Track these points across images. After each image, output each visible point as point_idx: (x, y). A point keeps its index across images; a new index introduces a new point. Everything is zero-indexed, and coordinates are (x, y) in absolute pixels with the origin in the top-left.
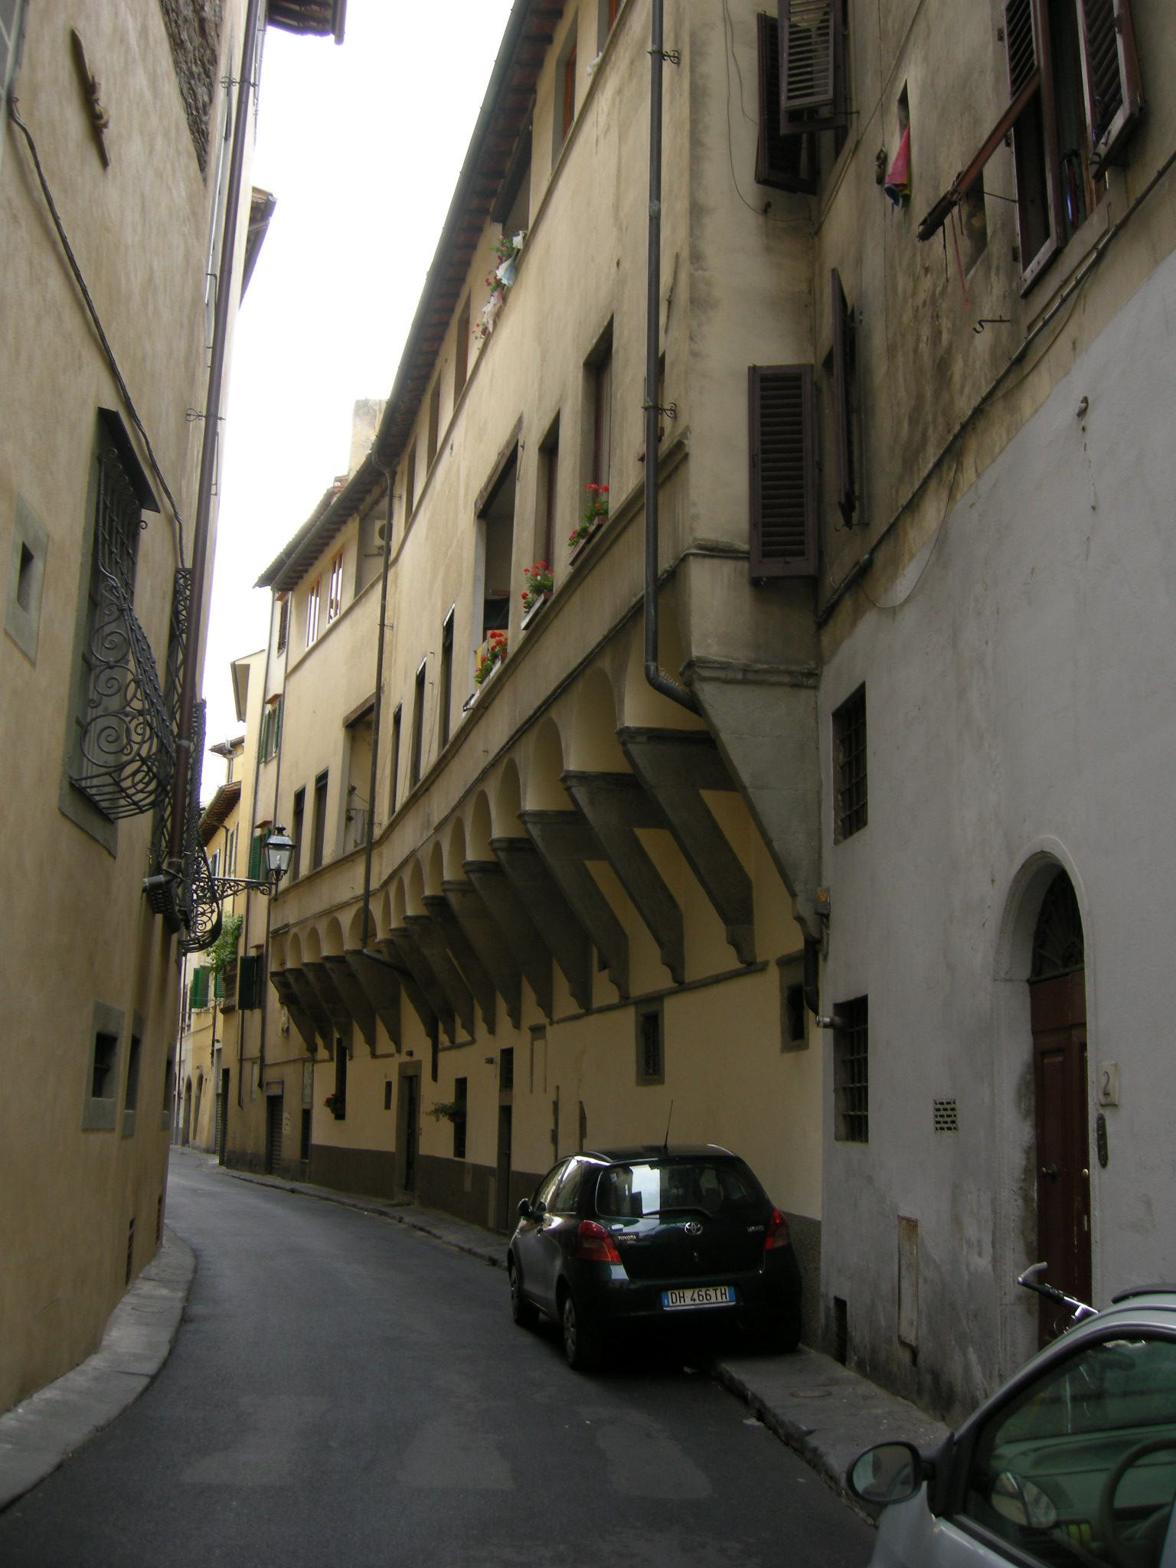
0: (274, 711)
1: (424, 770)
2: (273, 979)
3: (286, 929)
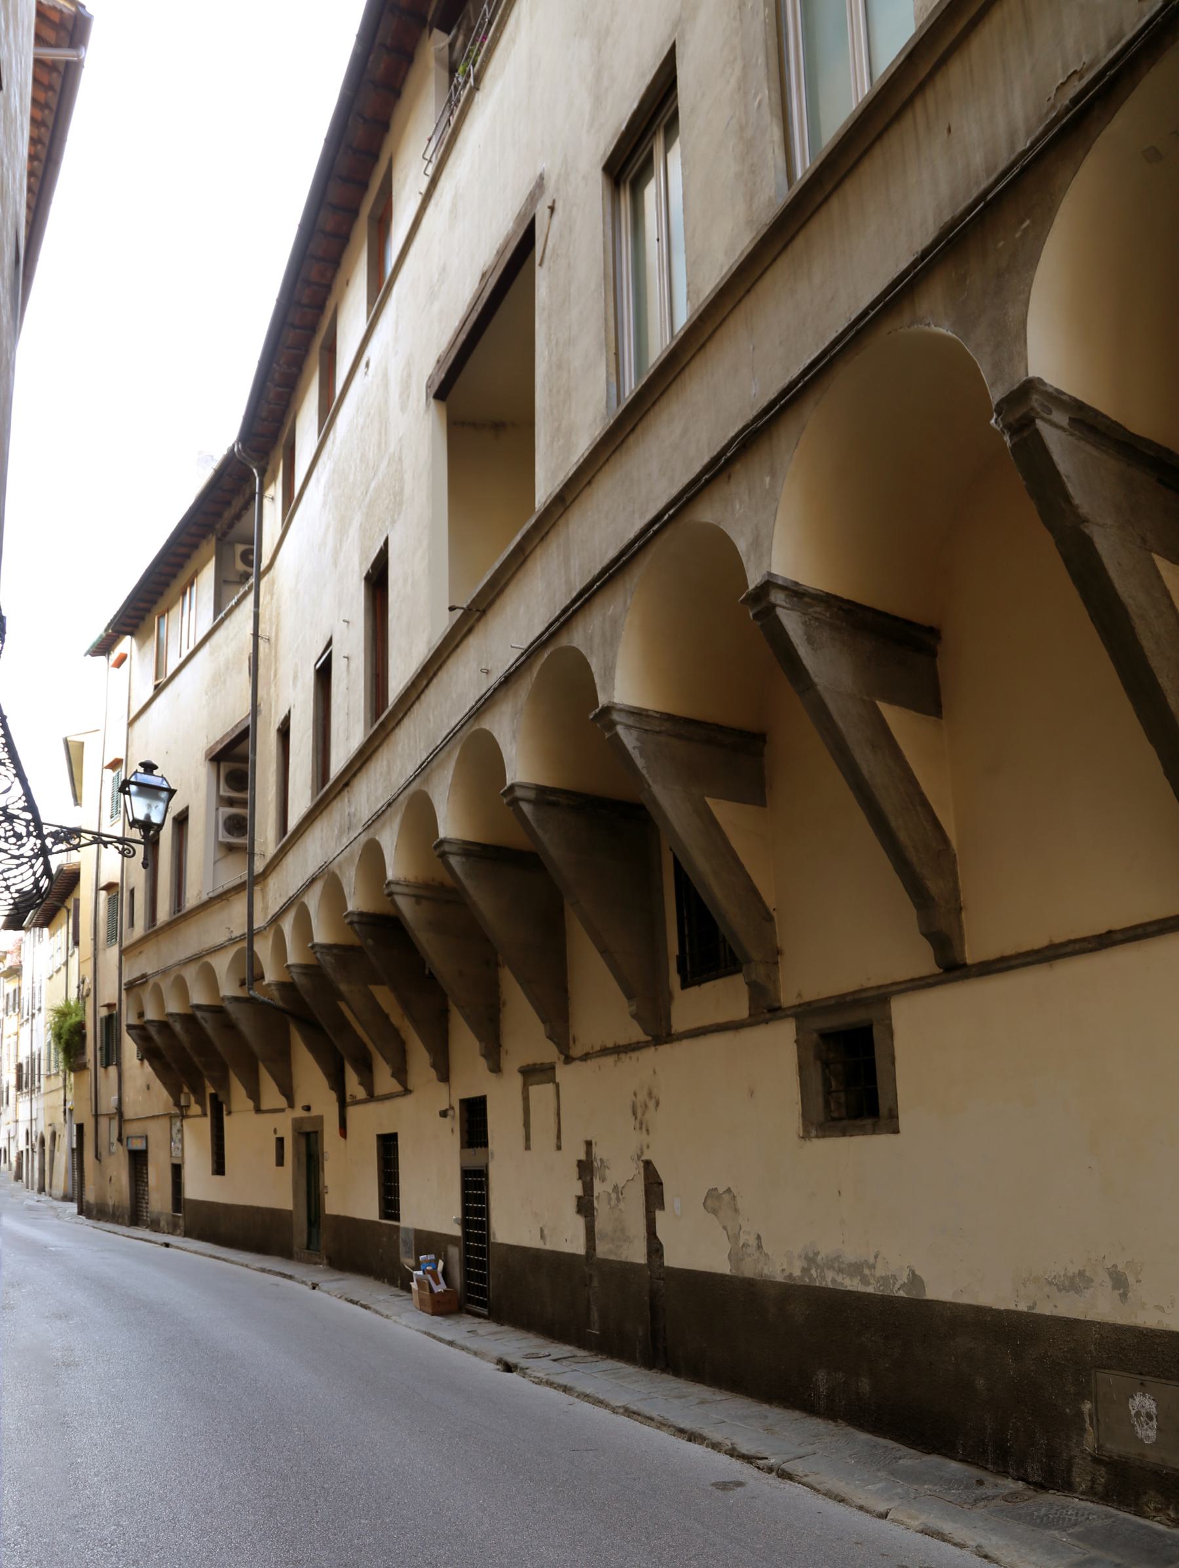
2: (130, 1031)
3: (144, 980)
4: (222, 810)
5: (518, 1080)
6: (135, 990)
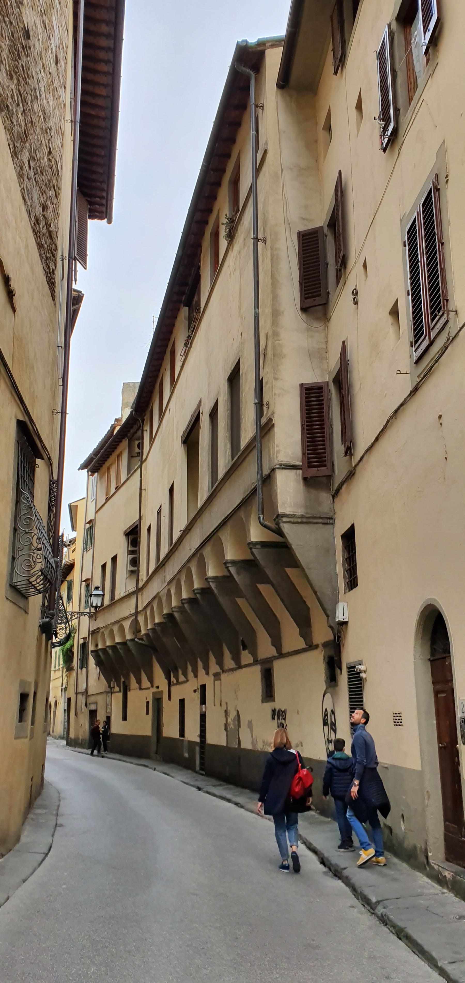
0: (90, 527)
1: (162, 557)
2: (92, 654)
4: (129, 556)
5: (213, 677)
6: (95, 635)
